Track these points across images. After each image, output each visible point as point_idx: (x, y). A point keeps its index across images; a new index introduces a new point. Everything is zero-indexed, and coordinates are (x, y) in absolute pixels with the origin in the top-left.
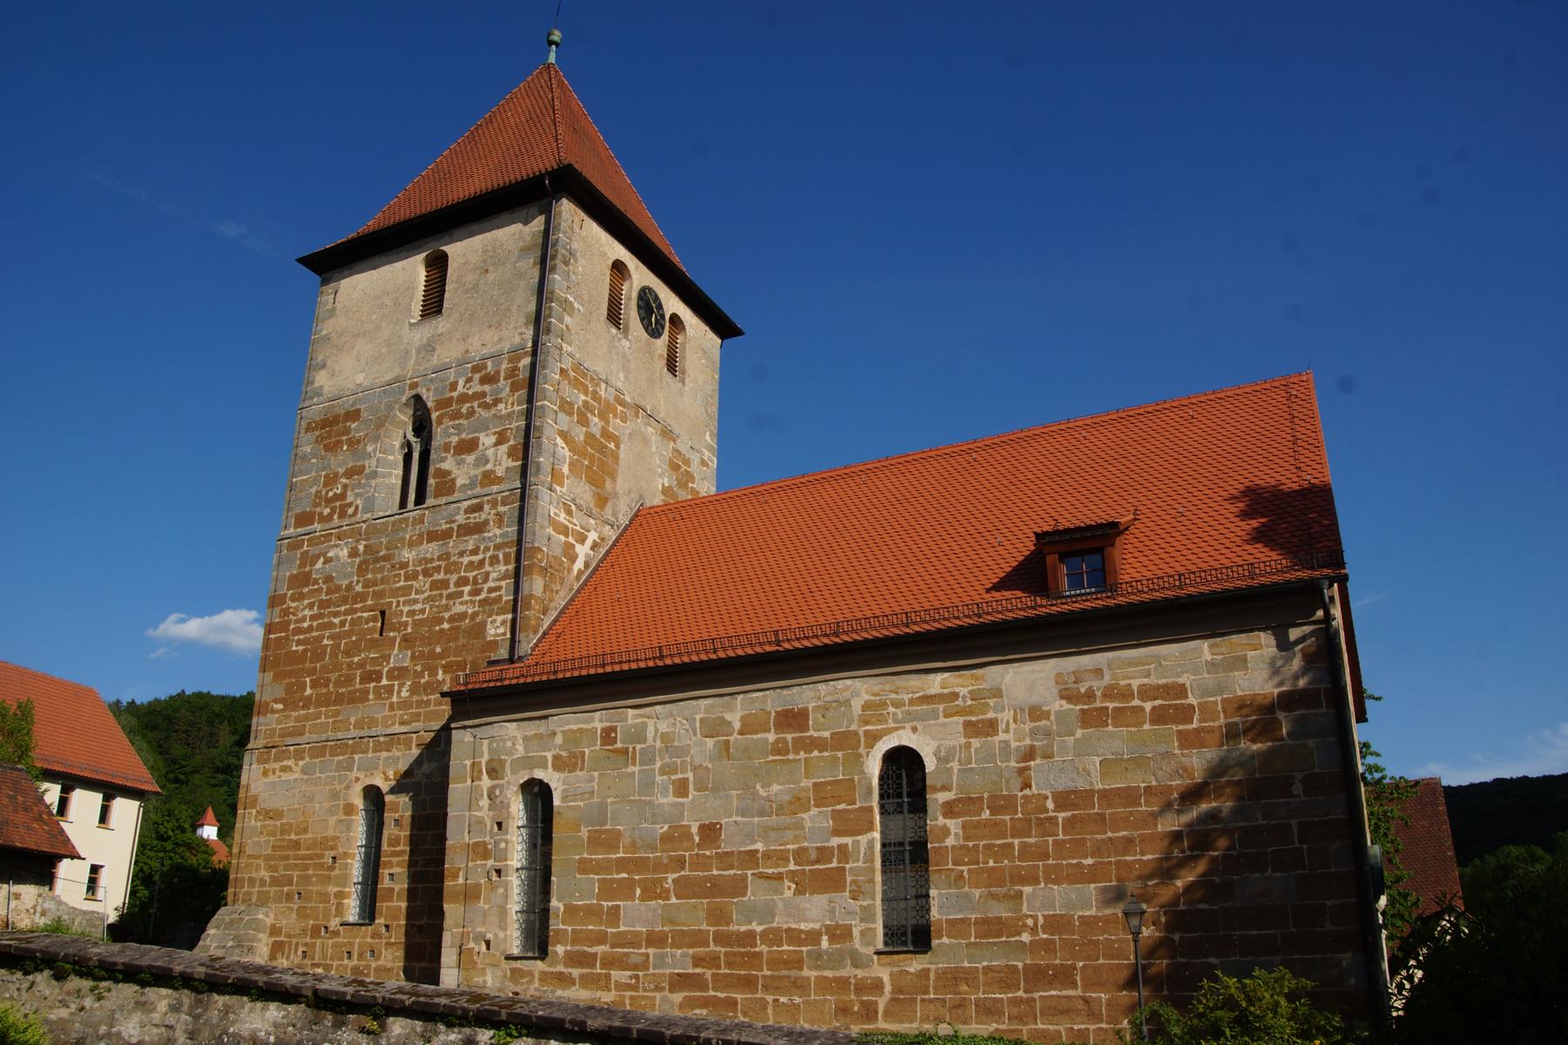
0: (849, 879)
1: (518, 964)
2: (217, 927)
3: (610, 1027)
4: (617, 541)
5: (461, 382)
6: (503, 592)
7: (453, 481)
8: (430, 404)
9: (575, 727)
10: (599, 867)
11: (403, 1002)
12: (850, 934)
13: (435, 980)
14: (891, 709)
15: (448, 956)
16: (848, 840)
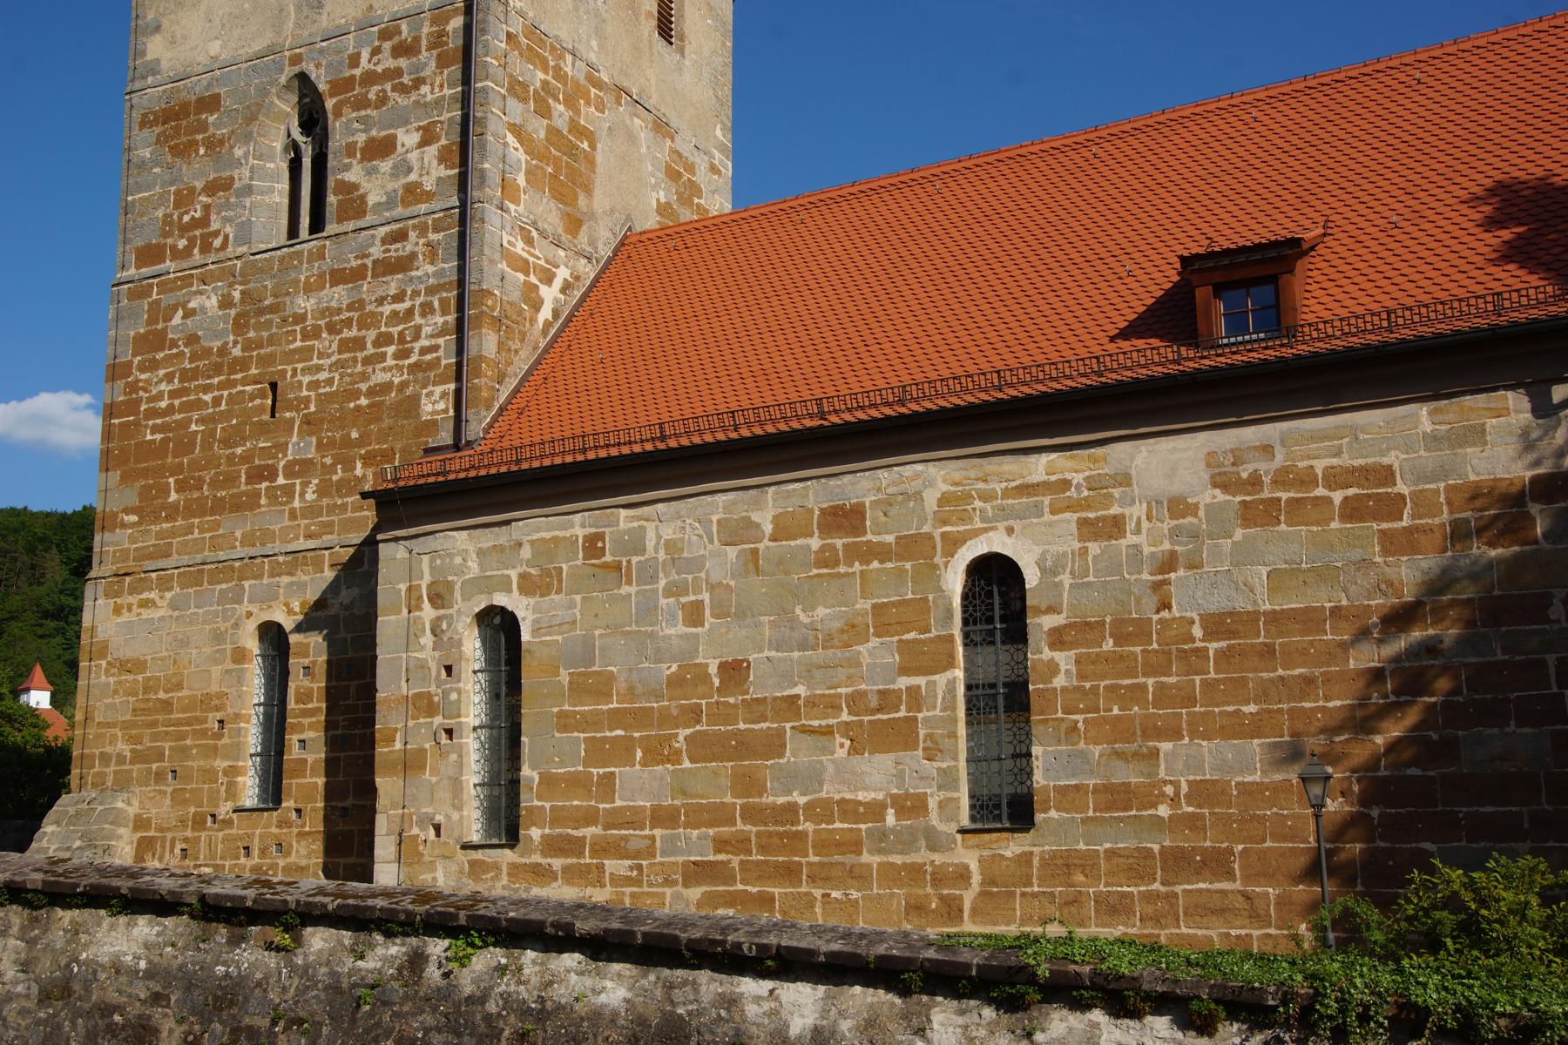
0: (922, 733)
1: (479, 855)
2: (58, 823)
3: (606, 931)
4: (596, 280)
5: (365, 55)
6: (441, 353)
7: (363, 197)
8: (322, 87)
9: (547, 535)
10: (587, 722)
11: (324, 906)
12: (925, 807)
13: (367, 876)
14: (978, 504)
15: (384, 847)
16: (921, 681)
